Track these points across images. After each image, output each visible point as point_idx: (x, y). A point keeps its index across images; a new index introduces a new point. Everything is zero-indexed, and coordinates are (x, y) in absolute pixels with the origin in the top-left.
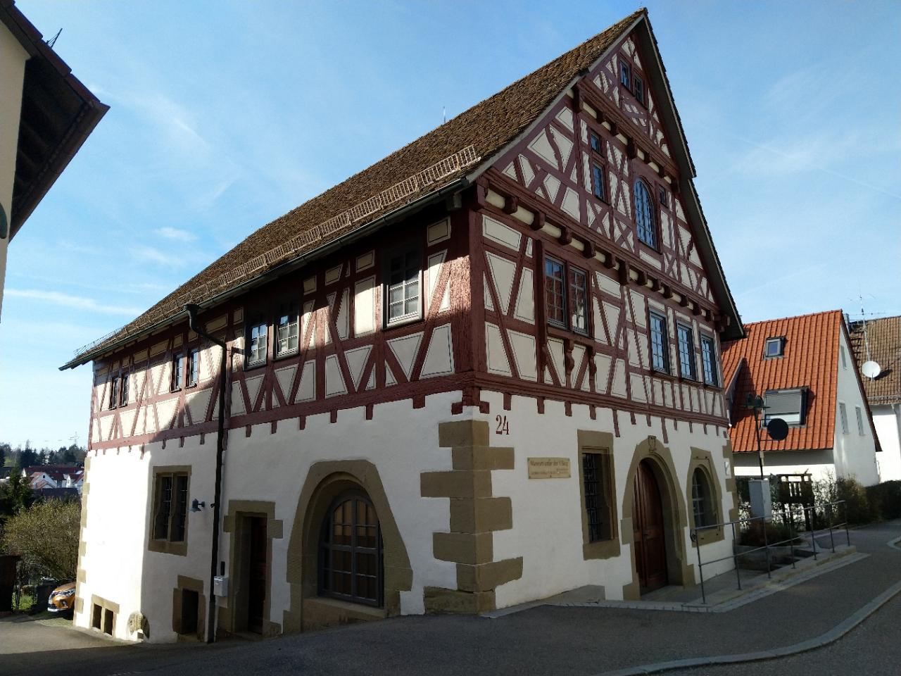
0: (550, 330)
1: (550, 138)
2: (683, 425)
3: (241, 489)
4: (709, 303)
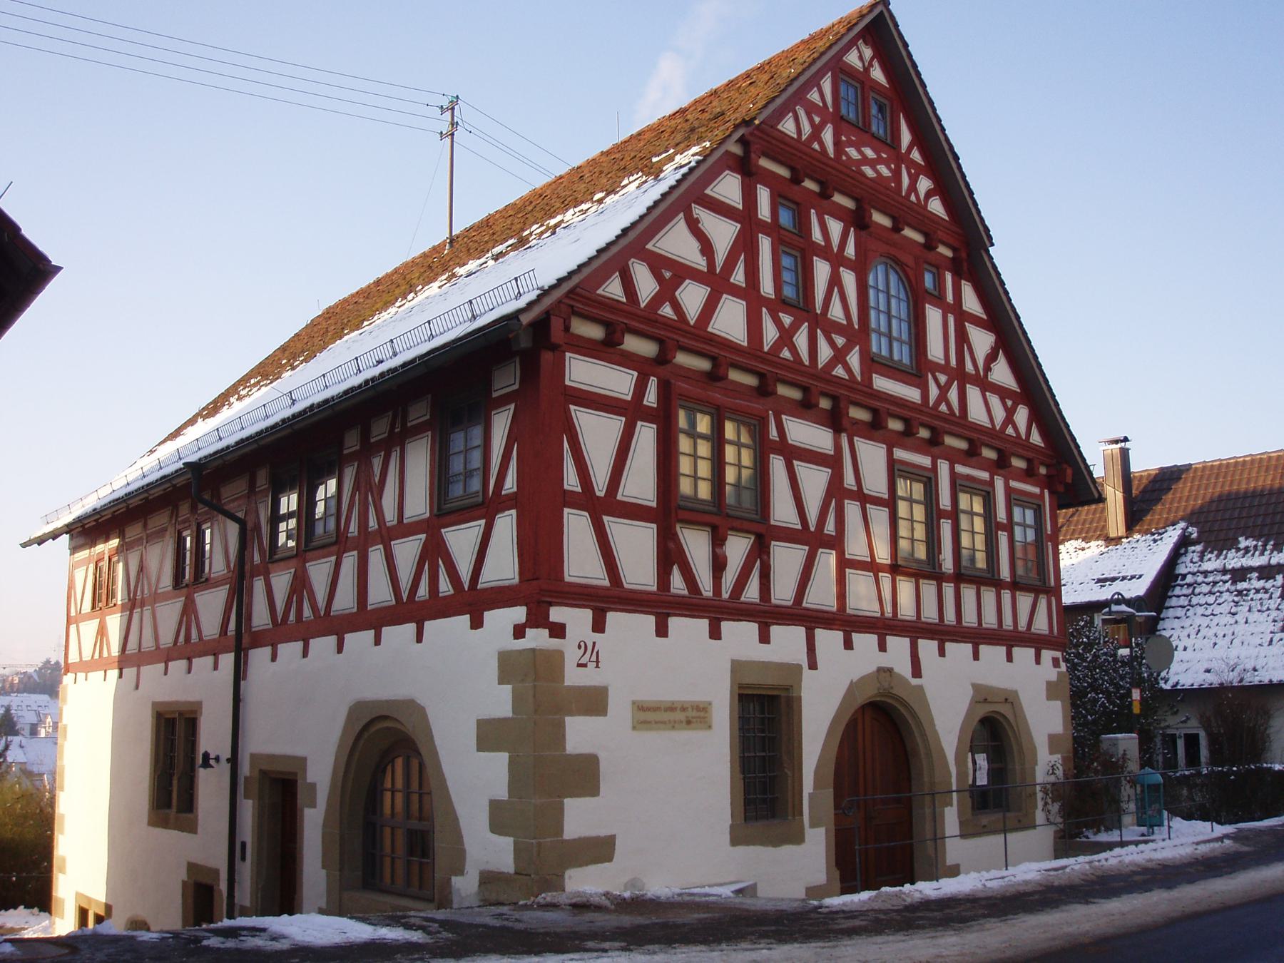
2: (959, 651)
3: (259, 738)
4: (1034, 448)
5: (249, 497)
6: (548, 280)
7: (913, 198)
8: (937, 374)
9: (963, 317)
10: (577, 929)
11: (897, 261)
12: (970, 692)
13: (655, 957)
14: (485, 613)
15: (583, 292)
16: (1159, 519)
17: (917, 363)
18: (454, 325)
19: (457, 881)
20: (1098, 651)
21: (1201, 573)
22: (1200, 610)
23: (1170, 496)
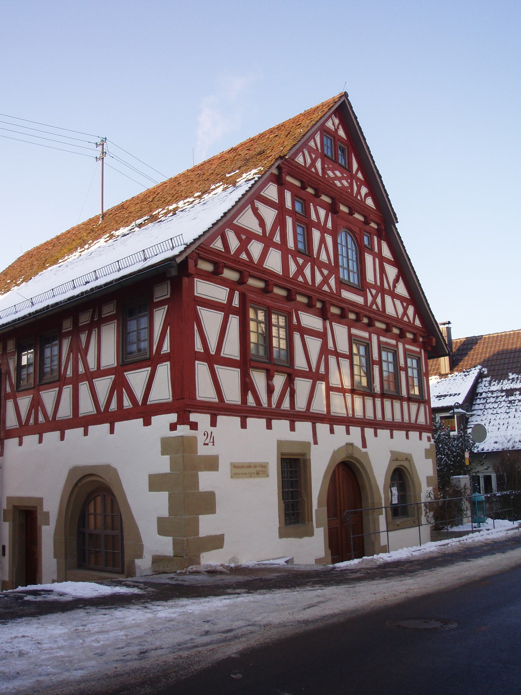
0: (253, 364)
1: (255, 211)
2: (383, 433)
4: (417, 328)
5: (2, 356)
6: (189, 240)
7: (359, 197)
8: (371, 289)
9: (382, 260)
10: (217, 584)
11: (351, 230)
12: (389, 455)
13: (265, 596)
14: (153, 418)
15: (204, 246)
16: (467, 364)
17: (361, 284)
18: (133, 263)
19: (138, 562)
20: (440, 433)
21: (490, 392)
22: (490, 411)
23: (472, 352)
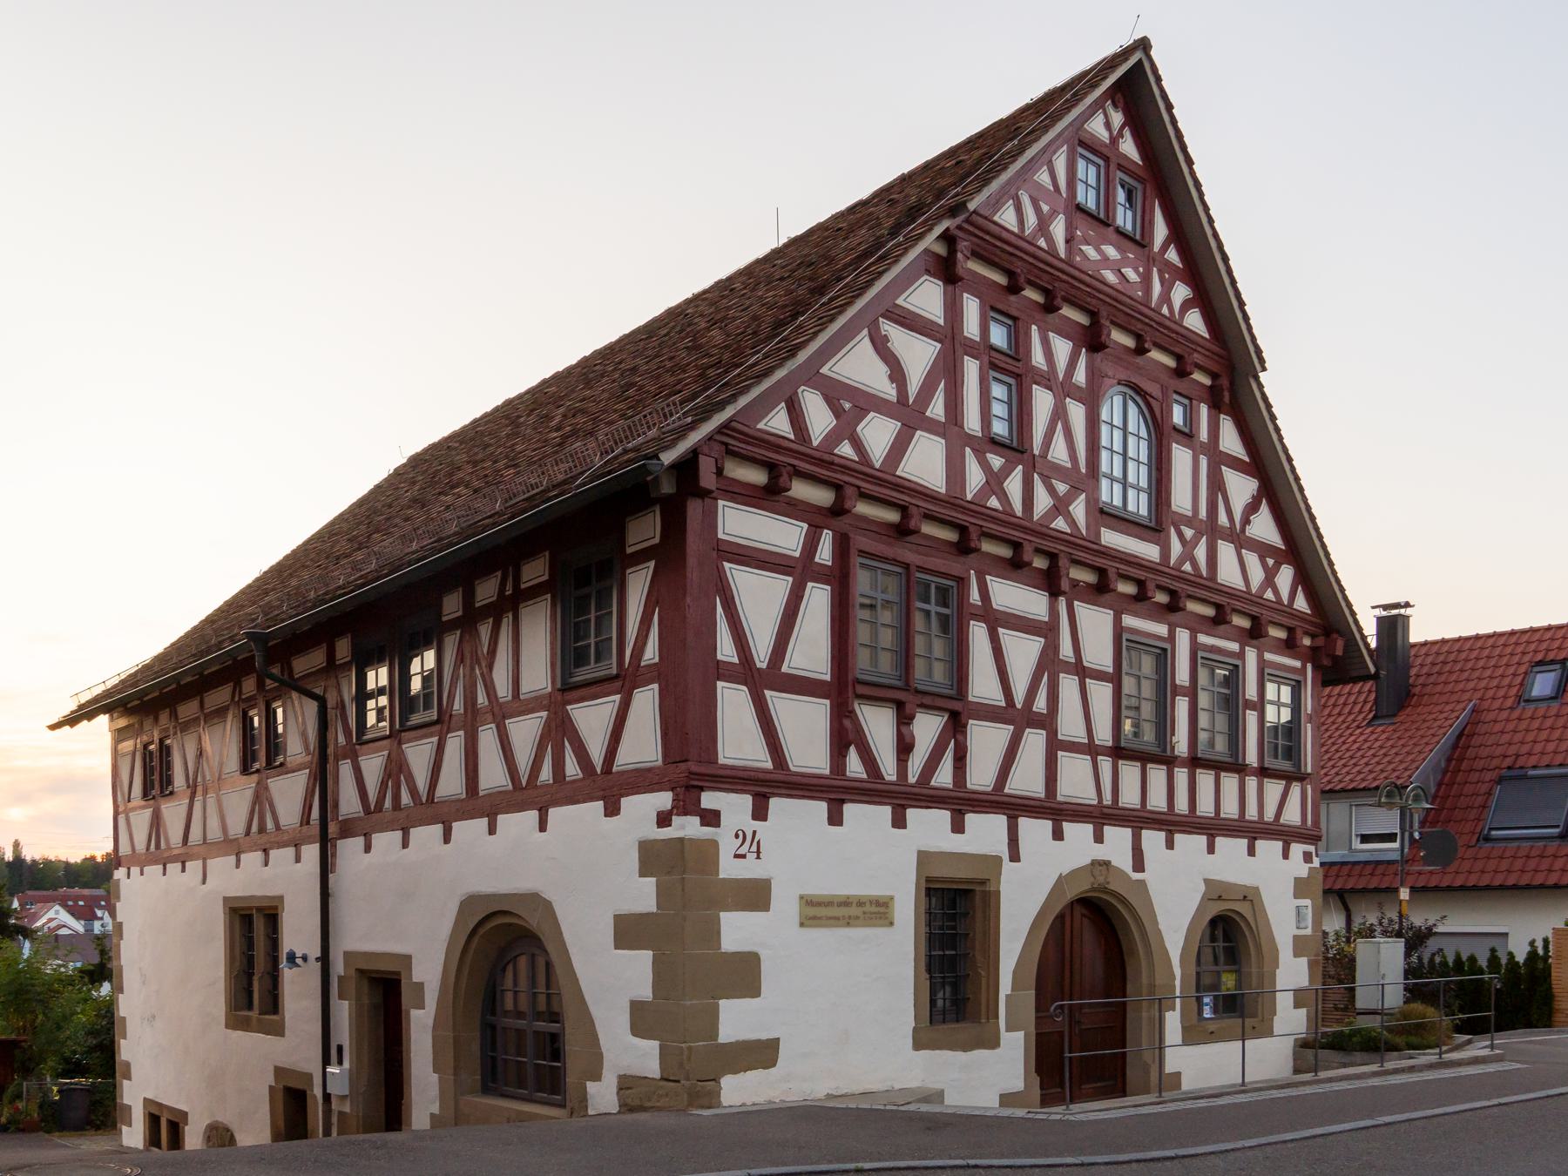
9: (1218, 460)
12: (1202, 888)
